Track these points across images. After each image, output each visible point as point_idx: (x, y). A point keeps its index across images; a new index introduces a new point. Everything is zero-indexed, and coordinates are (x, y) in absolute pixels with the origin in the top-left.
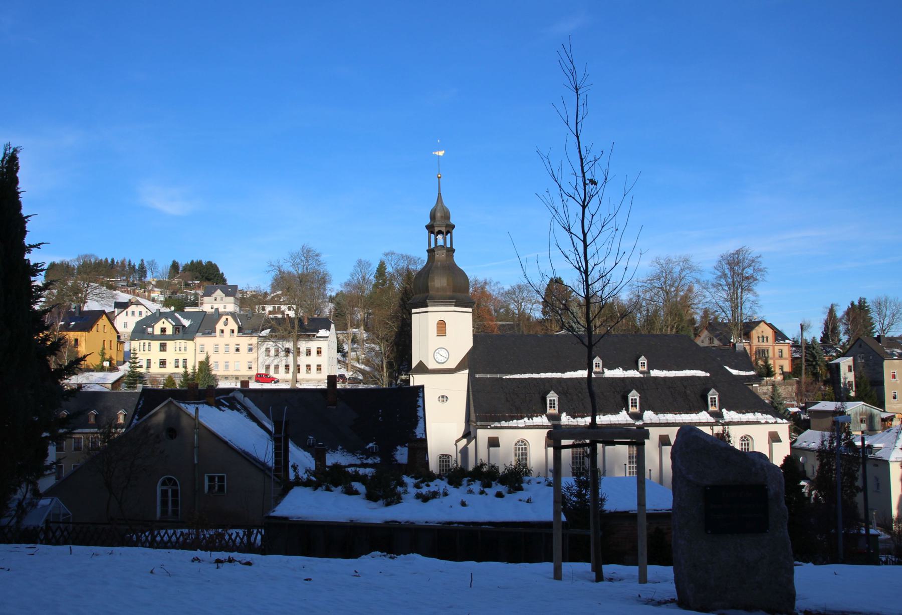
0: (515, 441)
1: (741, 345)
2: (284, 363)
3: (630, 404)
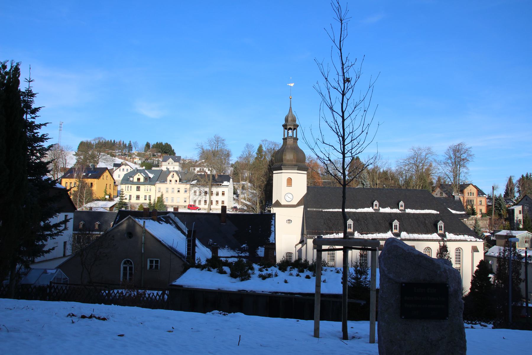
1: (457, 196)
2: (204, 199)
3: (393, 228)
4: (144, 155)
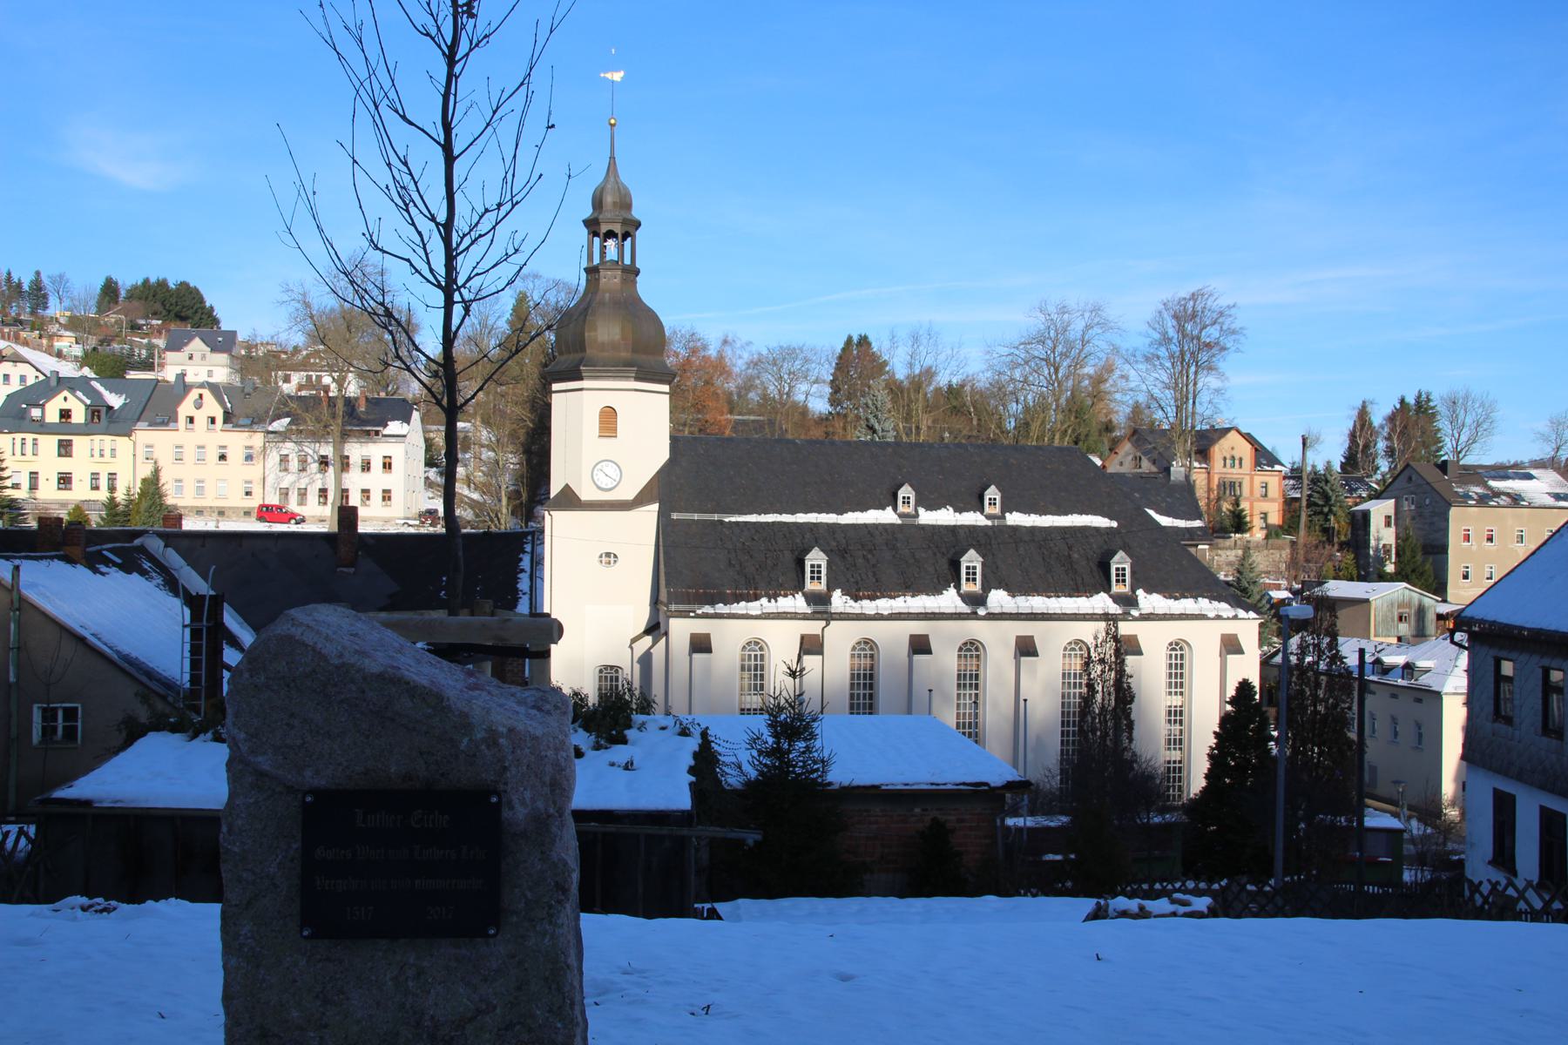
0: (743, 642)
2: (319, 485)
3: (964, 576)
4: (96, 322)
